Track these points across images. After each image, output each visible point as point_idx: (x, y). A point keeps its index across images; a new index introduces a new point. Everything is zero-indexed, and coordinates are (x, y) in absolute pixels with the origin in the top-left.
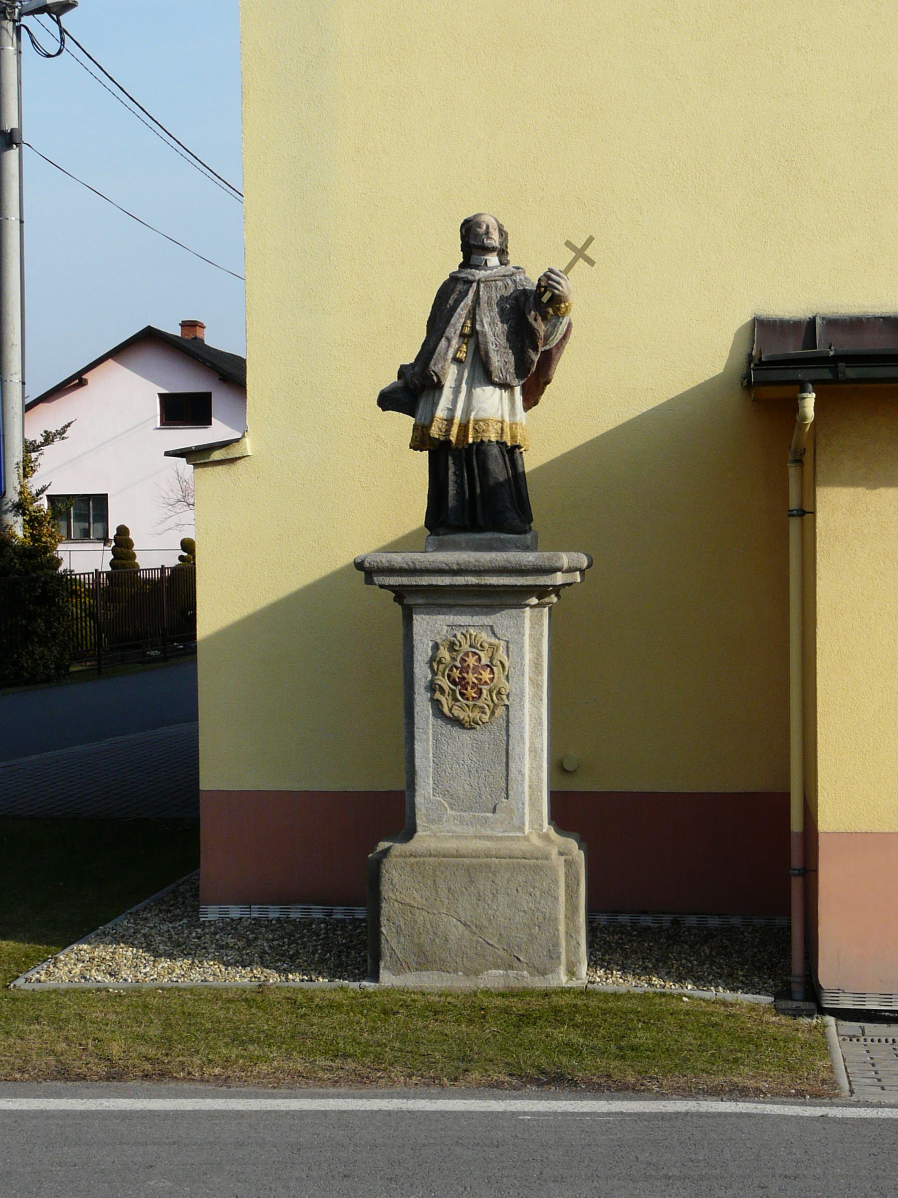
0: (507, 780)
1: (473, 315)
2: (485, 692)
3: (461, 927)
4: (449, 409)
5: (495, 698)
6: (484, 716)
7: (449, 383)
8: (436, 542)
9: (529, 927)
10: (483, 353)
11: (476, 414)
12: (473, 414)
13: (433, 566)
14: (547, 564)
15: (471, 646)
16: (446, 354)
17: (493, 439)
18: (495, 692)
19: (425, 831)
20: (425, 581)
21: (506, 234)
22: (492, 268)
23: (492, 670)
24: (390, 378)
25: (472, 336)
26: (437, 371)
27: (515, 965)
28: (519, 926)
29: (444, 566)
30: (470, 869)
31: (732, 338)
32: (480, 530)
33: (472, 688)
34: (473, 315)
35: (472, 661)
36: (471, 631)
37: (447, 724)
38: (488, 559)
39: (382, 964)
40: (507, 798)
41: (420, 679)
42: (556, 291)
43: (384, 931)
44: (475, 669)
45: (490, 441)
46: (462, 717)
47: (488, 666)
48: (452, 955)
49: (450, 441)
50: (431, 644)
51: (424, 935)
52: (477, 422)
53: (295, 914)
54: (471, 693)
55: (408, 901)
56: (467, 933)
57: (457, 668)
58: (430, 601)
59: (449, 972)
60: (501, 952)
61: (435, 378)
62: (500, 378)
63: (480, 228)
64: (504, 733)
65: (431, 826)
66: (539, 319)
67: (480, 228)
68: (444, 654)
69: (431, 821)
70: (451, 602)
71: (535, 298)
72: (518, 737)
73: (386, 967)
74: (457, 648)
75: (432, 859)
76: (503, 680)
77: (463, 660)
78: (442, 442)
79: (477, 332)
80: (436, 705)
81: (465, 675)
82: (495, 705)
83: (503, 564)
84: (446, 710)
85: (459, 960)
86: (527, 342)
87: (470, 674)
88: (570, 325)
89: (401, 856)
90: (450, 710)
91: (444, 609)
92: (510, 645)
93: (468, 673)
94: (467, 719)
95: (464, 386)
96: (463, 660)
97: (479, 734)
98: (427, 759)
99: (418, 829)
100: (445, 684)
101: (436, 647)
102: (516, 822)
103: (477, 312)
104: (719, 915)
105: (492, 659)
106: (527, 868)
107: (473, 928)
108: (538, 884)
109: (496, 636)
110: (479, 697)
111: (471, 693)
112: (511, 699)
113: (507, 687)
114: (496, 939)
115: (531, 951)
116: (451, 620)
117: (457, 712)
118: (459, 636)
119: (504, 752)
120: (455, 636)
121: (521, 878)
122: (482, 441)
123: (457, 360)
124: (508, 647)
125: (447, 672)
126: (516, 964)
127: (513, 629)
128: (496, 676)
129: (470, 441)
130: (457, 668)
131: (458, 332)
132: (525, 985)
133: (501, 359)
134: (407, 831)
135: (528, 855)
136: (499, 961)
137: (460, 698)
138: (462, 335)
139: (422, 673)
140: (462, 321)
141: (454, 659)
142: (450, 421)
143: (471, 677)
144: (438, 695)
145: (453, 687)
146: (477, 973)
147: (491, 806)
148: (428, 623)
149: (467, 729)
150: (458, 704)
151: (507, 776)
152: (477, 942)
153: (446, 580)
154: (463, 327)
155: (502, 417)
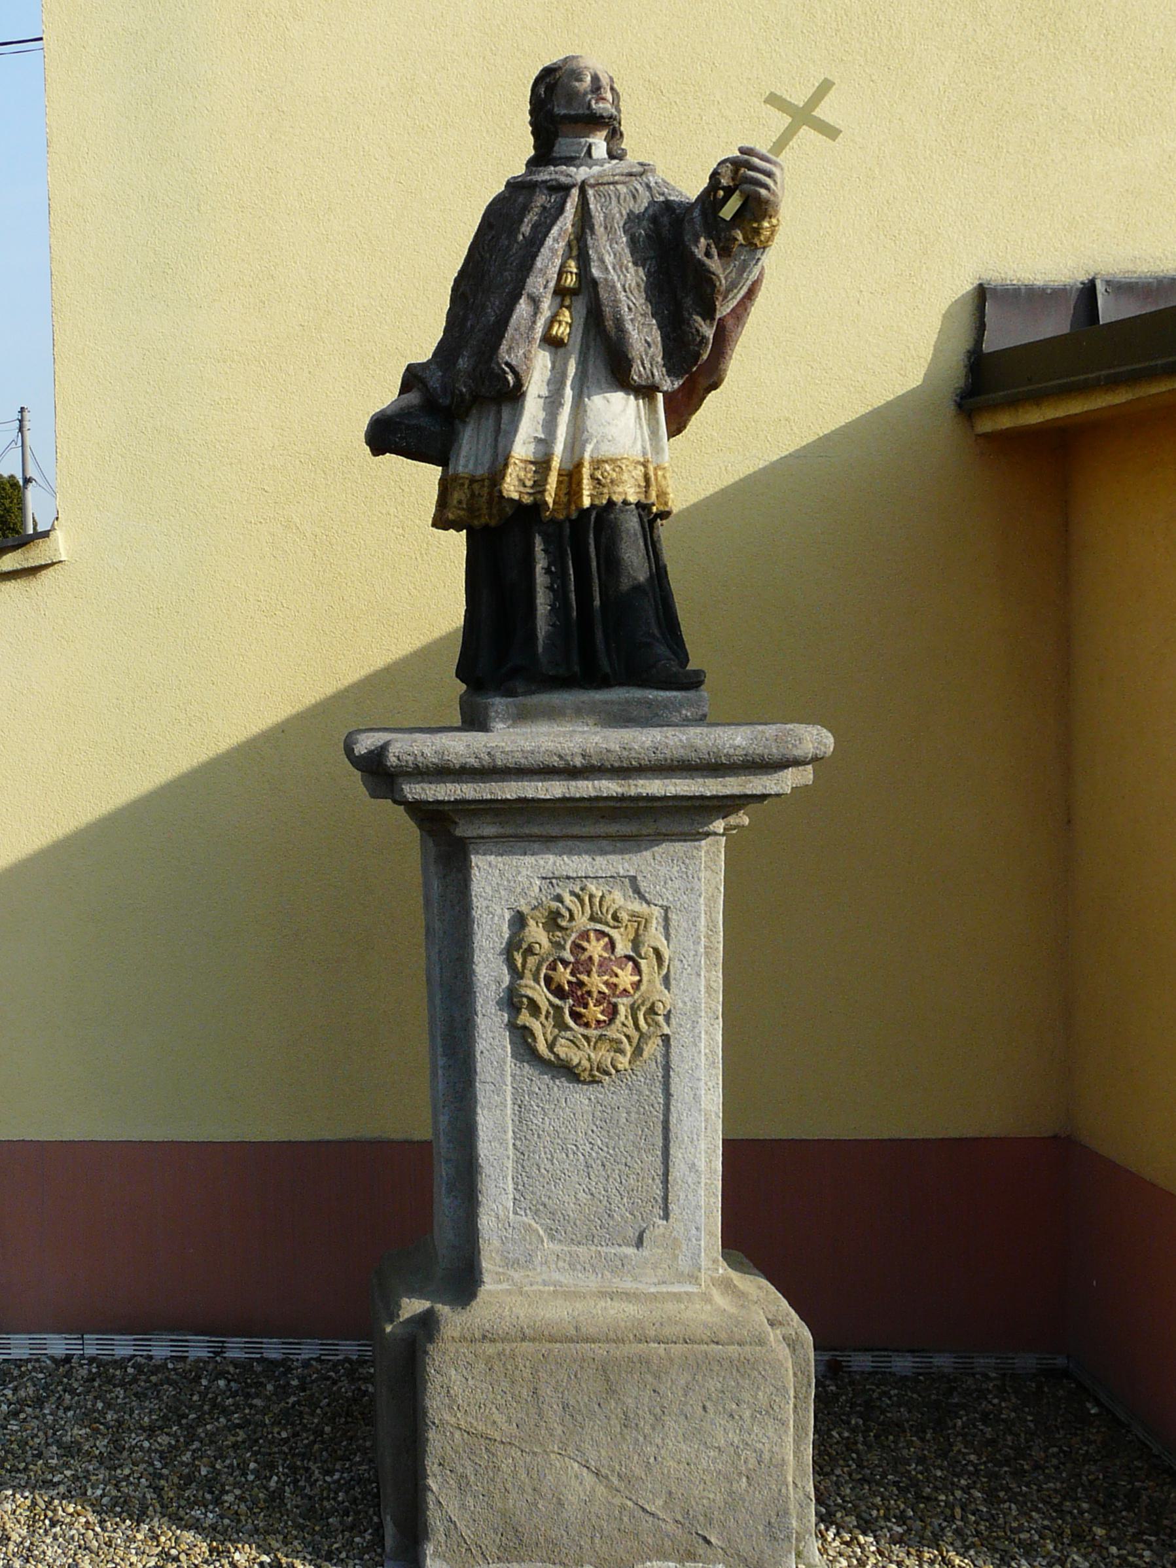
0: (666, 1182)
1: (579, 249)
2: (622, 1010)
4: (539, 441)
5: (642, 1022)
6: (620, 1058)
7: (536, 387)
8: (513, 710)
9: (726, 1478)
10: (609, 324)
11: (596, 448)
12: (589, 448)
13: (532, 761)
14: (775, 752)
15: (592, 919)
16: (532, 328)
18: (643, 1009)
19: (500, 1282)
20: (511, 790)
22: (600, 163)
23: (637, 966)
24: (385, 393)
25: (585, 293)
26: (514, 363)
28: (707, 1478)
29: (555, 761)
31: (937, 325)
32: (604, 683)
34: (579, 249)
35: (596, 949)
36: (592, 888)
37: (542, 1073)
38: (648, 744)
39: (430, 1549)
40: (666, 1217)
41: (487, 986)
42: (763, 192)
43: (434, 1487)
45: (625, 503)
46: (575, 1061)
47: (629, 958)
48: (573, 1533)
49: (546, 503)
50: (507, 916)
51: (514, 1494)
52: (597, 464)
53: (160, 1350)
54: (595, 1012)
55: (481, 1427)
56: (601, 1490)
57: (565, 963)
58: (509, 830)
60: (670, 1527)
61: (510, 378)
62: (640, 376)
63: (580, 80)
64: (659, 1090)
65: (511, 1273)
66: (714, 251)
67: (580, 80)
68: (537, 933)
70: (554, 830)
71: (704, 213)
72: (689, 1098)
73: (436, 1554)
74: (564, 924)
76: (658, 981)
77: (578, 948)
78: (527, 506)
79: (594, 283)
80: (522, 1038)
81: (584, 978)
82: (642, 1035)
83: (681, 753)
84: (542, 1047)
85: (585, 1543)
86: (688, 302)
87: (594, 975)
88: (761, 274)
89: (463, 1339)
90: (551, 1047)
91: (536, 846)
92: (673, 916)
93: (589, 974)
94: (585, 1063)
95: (568, 393)
96: (578, 948)
97: (610, 1093)
98: (502, 1142)
99: (486, 1278)
100: (541, 995)
101: (519, 921)
102: (684, 1265)
103: (590, 242)
104: (911, 1351)
105: (636, 943)
106: (726, 1364)
107: (615, 1480)
108: (746, 1396)
109: (642, 897)
110: (611, 1021)
112: (673, 1021)
113: (665, 998)
115: (732, 1523)
116: (549, 866)
117: (563, 1050)
118: (568, 898)
119: (659, 1129)
120: (559, 899)
121: (713, 1385)
122: (611, 503)
123: (552, 343)
124: (666, 919)
125: (544, 971)
126: (701, 1549)
127: (677, 884)
128: (645, 978)
129: (587, 502)
130: (565, 963)
131: (552, 285)
133: (644, 338)
134: (464, 1282)
135: (723, 1336)
136: (667, 1543)
137: (572, 1024)
138: (561, 292)
139: (489, 972)
140: (558, 262)
141: (559, 946)
142: (542, 465)
143: (596, 982)
145: (557, 1001)
147: (632, 1234)
148: (501, 874)
149: (584, 1082)
150: (568, 1034)
151: (666, 1173)
152: (623, 1507)
153: (555, 789)
154: (560, 274)
155: (644, 454)
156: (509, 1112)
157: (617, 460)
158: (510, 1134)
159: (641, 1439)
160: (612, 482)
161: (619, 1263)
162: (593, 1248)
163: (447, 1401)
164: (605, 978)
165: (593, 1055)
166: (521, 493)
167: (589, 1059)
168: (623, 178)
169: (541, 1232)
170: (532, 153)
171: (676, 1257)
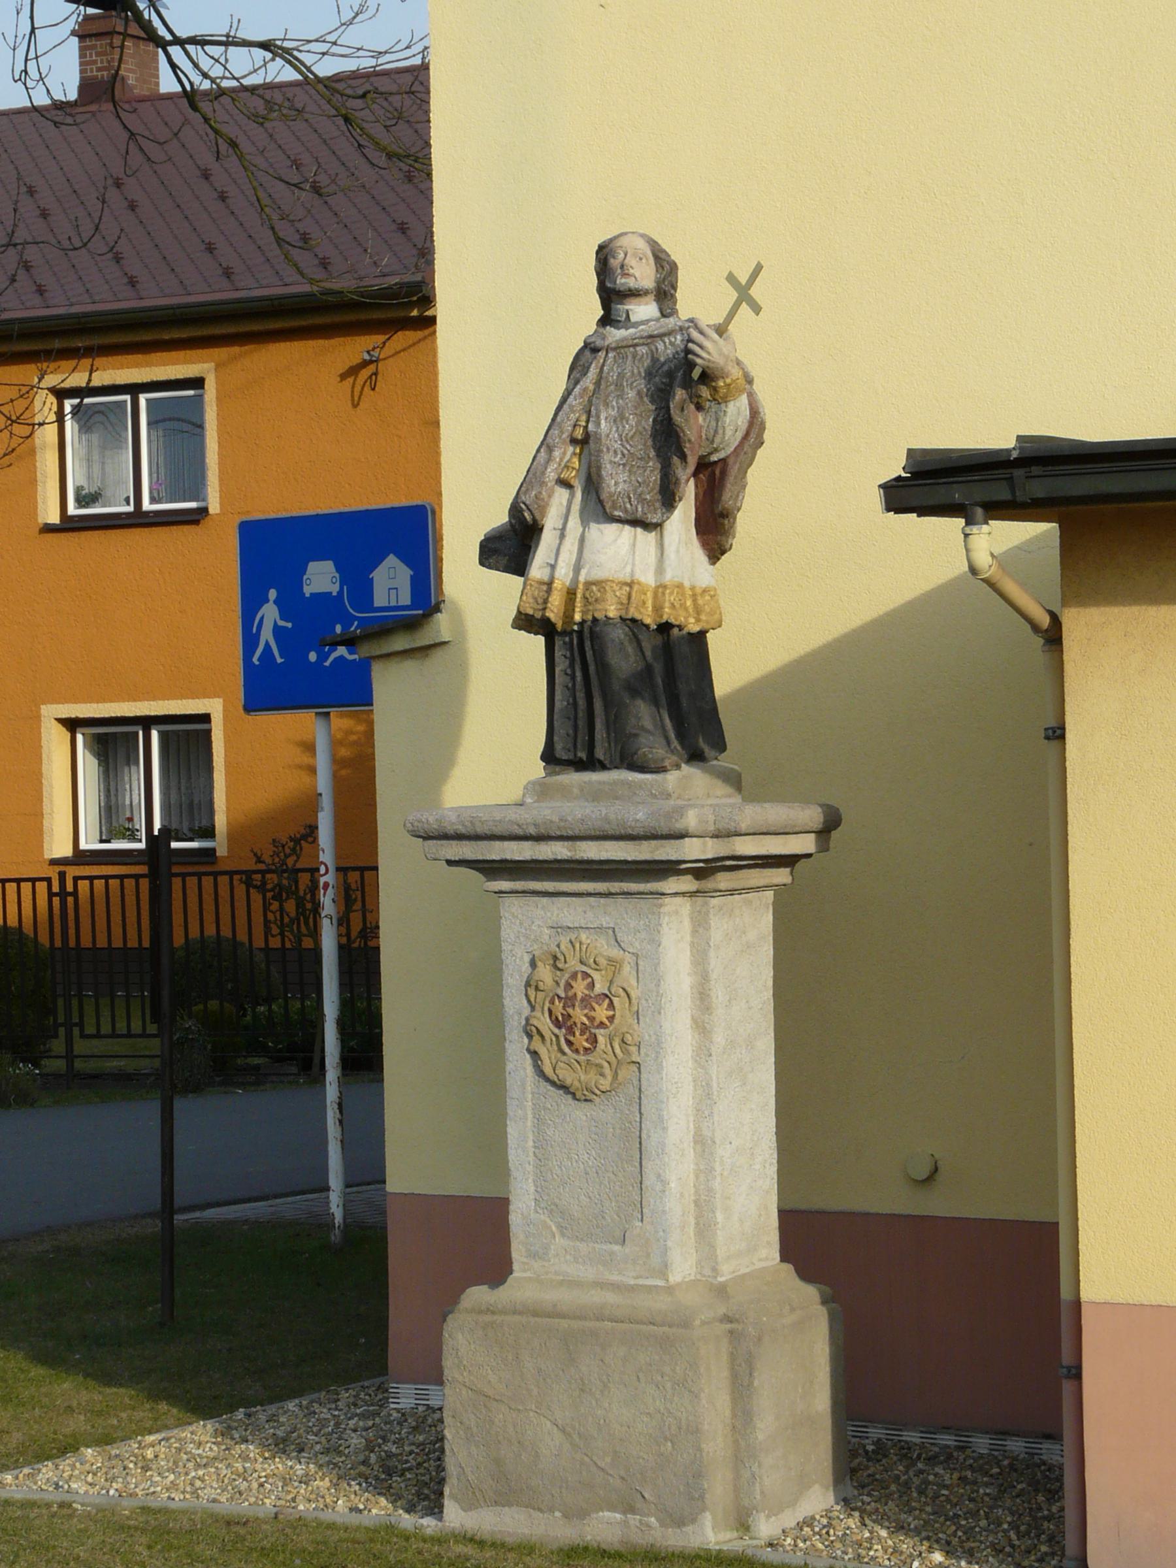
2: (601, 1039)
3: (558, 1436)
5: (617, 1047)
6: (602, 1081)
11: (588, 573)
17: (613, 612)
19: (525, 1271)
21: (674, 267)
27: (638, 1506)
30: (573, 1333)
33: (582, 1033)
35: (580, 988)
41: (512, 1016)
44: (586, 1002)
52: (588, 584)
54: (581, 1041)
59: (540, 1510)
67: (614, 258)
69: (534, 1255)
73: (454, 1497)
75: (517, 1318)
77: (569, 986)
81: (570, 1010)
84: (548, 1070)
87: (577, 1008)
92: (641, 963)
94: (576, 1083)
96: (569, 986)
99: (515, 1266)
107: (575, 1437)
108: (667, 1369)
111: (581, 1041)
114: (608, 1459)
122: (595, 620)
127: (643, 935)
128: (618, 1014)
129: (578, 617)
132: (651, 1540)
134: (497, 1269)
139: (515, 1004)
143: (579, 1015)
144: (537, 1044)
145: (556, 1031)
146: (582, 1514)
147: (618, 1234)
148: (521, 924)
152: (582, 1463)
156: (529, 1124)
157: (602, 582)
158: (531, 1143)
159: (594, 1403)
160: (596, 600)
161: (608, 1258)
162: (591, 1245)
163: (456, 1361)
164: (586, 1011)
165: (583, 1078)
166: (535, 610)
167: (579, 1081)
168: (641, 341)
169: (554, 1228)
170: (602, 312)
171: (648, 1255)
